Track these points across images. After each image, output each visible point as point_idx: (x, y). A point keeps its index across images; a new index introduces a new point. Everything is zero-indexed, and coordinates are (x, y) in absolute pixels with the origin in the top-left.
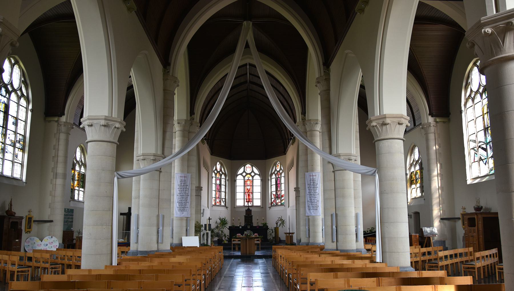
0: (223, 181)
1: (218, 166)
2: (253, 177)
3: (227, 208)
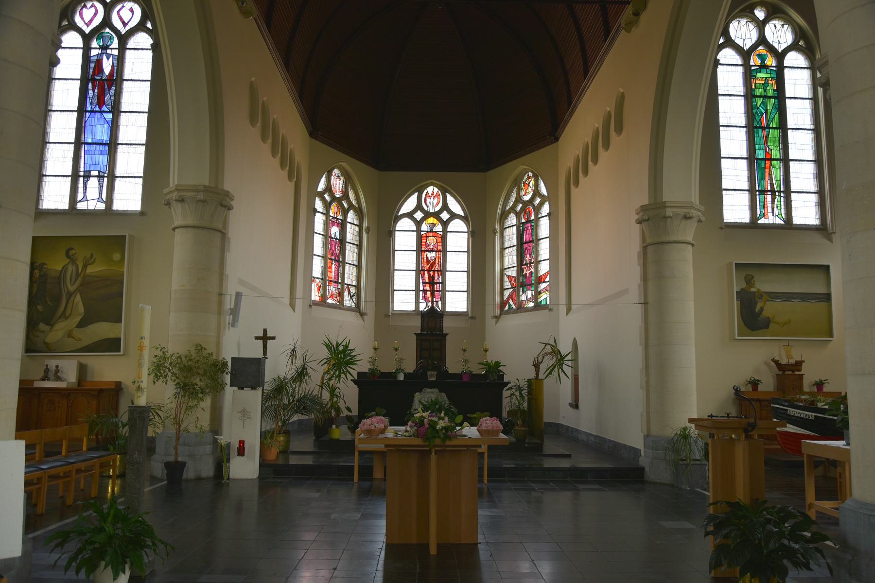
0: (351, 234)
1: (338, 185)
2: (445, 224)
3: (362, 315)
